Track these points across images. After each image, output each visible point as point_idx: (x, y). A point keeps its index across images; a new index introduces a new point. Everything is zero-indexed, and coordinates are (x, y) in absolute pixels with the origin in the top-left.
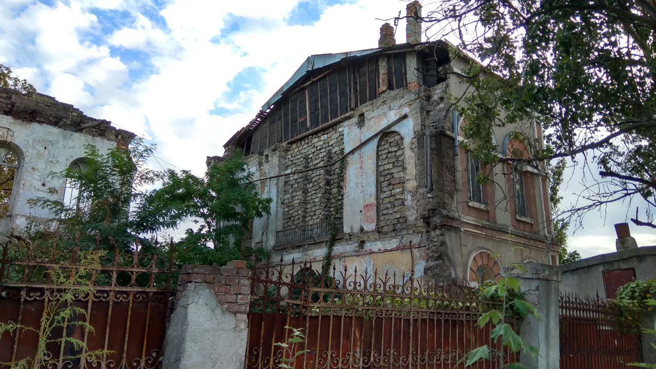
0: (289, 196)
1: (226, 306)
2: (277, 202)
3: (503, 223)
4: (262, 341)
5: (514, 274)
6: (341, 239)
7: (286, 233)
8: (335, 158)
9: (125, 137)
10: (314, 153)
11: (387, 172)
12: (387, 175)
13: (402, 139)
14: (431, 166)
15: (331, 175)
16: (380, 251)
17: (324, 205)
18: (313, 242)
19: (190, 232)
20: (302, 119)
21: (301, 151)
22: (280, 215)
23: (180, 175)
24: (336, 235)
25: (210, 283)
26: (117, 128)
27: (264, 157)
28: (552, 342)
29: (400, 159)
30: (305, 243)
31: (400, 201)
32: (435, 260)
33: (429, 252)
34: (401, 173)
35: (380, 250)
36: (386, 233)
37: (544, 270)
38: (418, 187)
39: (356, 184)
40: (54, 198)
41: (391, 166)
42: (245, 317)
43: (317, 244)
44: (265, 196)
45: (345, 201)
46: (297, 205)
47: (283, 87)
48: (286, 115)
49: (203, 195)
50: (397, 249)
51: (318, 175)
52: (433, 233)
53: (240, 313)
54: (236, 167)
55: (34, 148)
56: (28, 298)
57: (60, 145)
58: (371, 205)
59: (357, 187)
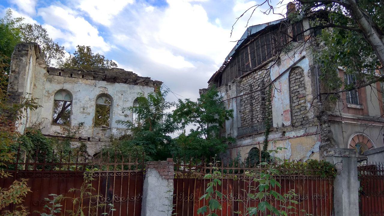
0: (243, 107)
1: (164, 176)
2: (237, 111)
3: (374, 115)
4: (184, 190)
5: (330, 154)
6: (272, 131)
7: (243, 128)
8: (267, 84)
9: (157, 84)
10: (255, 82)
11: (295, 91)
12: (296, 92)
13: (303, 70)
14: (319, 86)
15: (265, 94)
16: (294, 137)
17: (262, 112)
18: (257, 133)
19: (192, 130)
20: (247, 63)
21: (248, 82)
22: (239, 118)
23: (184, 102)
24: (269, 129)
25: (156, 168)
26: (154, 80)
27: (228, 87)
28: (352, 190)
29: (303, 82)
30: (253, 134)
31: (304, 107)
32: (326, 142)
33: (322, 137)
34: (304, 91)
35: (294, 136)
36: (297, 127)
37: (345, 152)
38: (314, 99)
39: (278, 99)
40: (126, 119)
41: (297, 87)
42: (172, 181)
43: (260, 134)
44: (230, 108)
45: (273, 109)
46: (248, 112)
47: (235, 46)
48: (238, 62)
49: (197, 111)
50: (304, 136)
51: (258, 95)
52: (324, 125)
53: (170, 179)
54: (214, 94)
55: (117, 95)
56: (93, 176)
57: (129, 92)
58: (287, 110)
59: (279, 101)
